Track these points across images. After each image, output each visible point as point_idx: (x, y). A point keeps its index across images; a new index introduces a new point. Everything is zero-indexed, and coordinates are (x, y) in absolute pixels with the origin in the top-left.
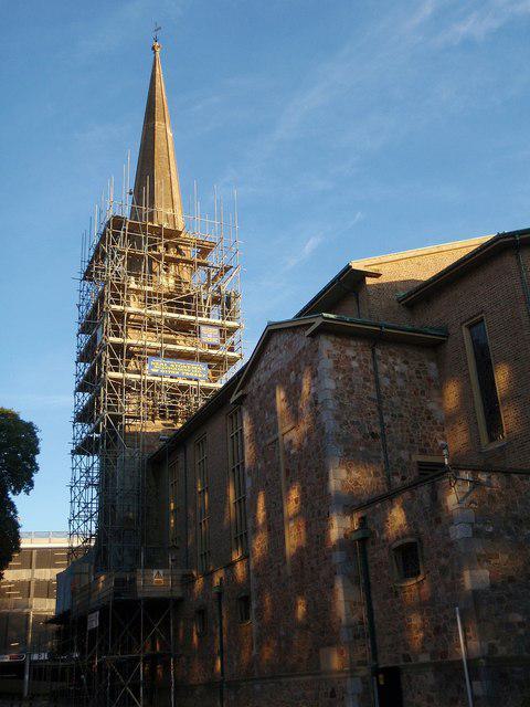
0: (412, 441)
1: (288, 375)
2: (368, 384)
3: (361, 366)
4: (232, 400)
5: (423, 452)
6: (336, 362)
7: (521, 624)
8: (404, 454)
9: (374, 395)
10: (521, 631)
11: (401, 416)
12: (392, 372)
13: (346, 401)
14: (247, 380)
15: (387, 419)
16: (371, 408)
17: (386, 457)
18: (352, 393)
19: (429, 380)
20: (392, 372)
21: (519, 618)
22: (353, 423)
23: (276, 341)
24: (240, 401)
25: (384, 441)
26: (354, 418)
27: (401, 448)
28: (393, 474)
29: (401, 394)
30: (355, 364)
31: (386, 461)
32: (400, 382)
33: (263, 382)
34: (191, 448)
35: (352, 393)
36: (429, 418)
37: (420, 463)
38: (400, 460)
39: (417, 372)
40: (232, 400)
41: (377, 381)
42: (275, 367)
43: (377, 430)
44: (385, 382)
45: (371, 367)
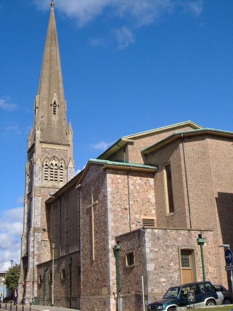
0: (141, 211)
1: (96, 182)
2: (125, 189)
3: (123, 181)
4: (77, 187)
5: (145, 215)
6: (112, 180)
7: (164, 282)
8: (137, 216)
9: (127, 193)
10: (164, 284)
11: (137, 201)
12: (135, 183)
13: (115, 196)
14: (86, 173)
15: (131, 202)
16: (126, 198)
17: (130, 217)
18: (118, 192)
19: (150, 186)
20: (135, 183)
21: (164, 280)
22: (118, 204)
23: (92, 167)
24: (80, 188)
25: (129, 211)
26: (118, 202)
27: (136, 213)
28: (133, 224)
29: (138, 192)
30: (120, 181)
31: (130, 219)
32: (138, 187)
33: (87, 182)
34: (63, 200)
35: (118, 192)
36: (149, 201)
37: (144, 219)
38: (136, 218)
39: (145, 183)
40: (77, 187)
41: (128, 187)
42: (92, 177)
43: (127, 207)
44: (132, 187)
45: (126, 181)
